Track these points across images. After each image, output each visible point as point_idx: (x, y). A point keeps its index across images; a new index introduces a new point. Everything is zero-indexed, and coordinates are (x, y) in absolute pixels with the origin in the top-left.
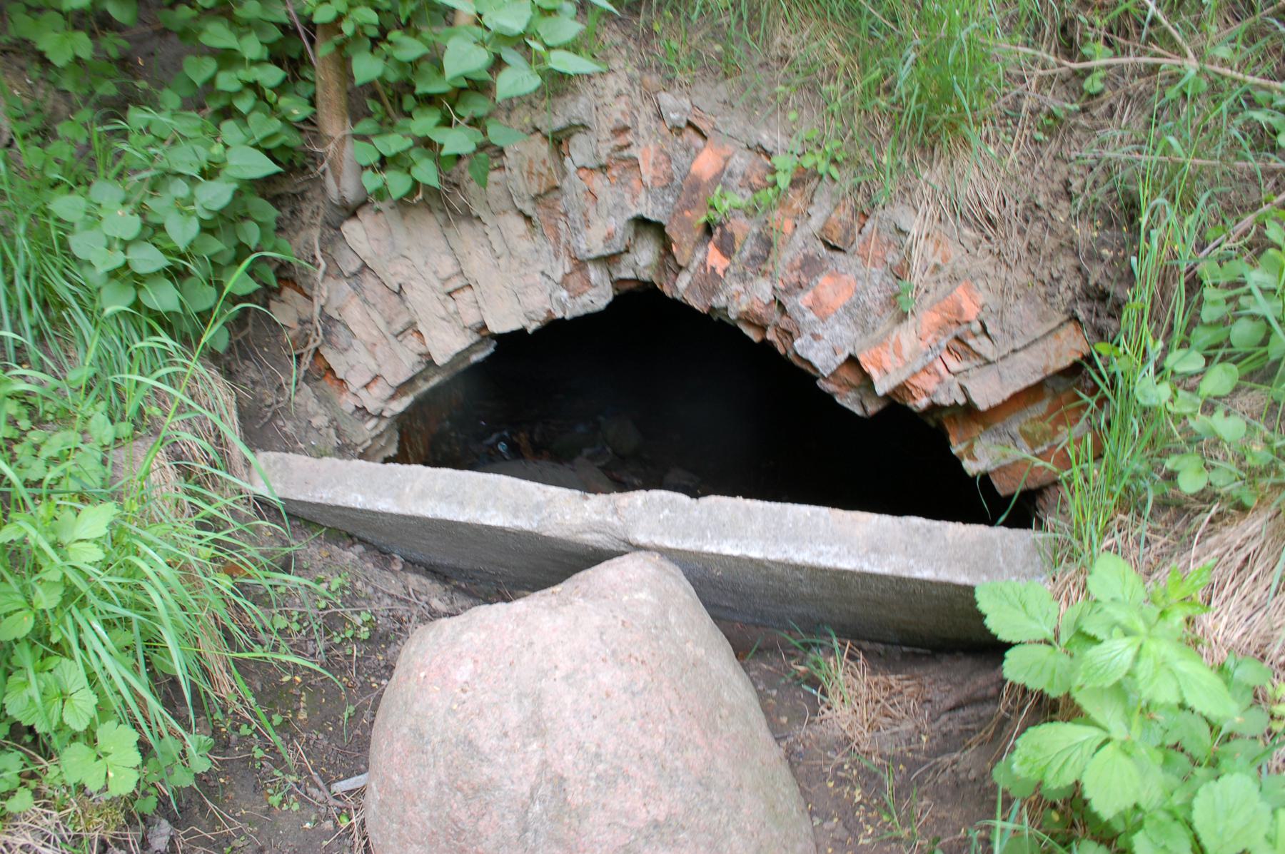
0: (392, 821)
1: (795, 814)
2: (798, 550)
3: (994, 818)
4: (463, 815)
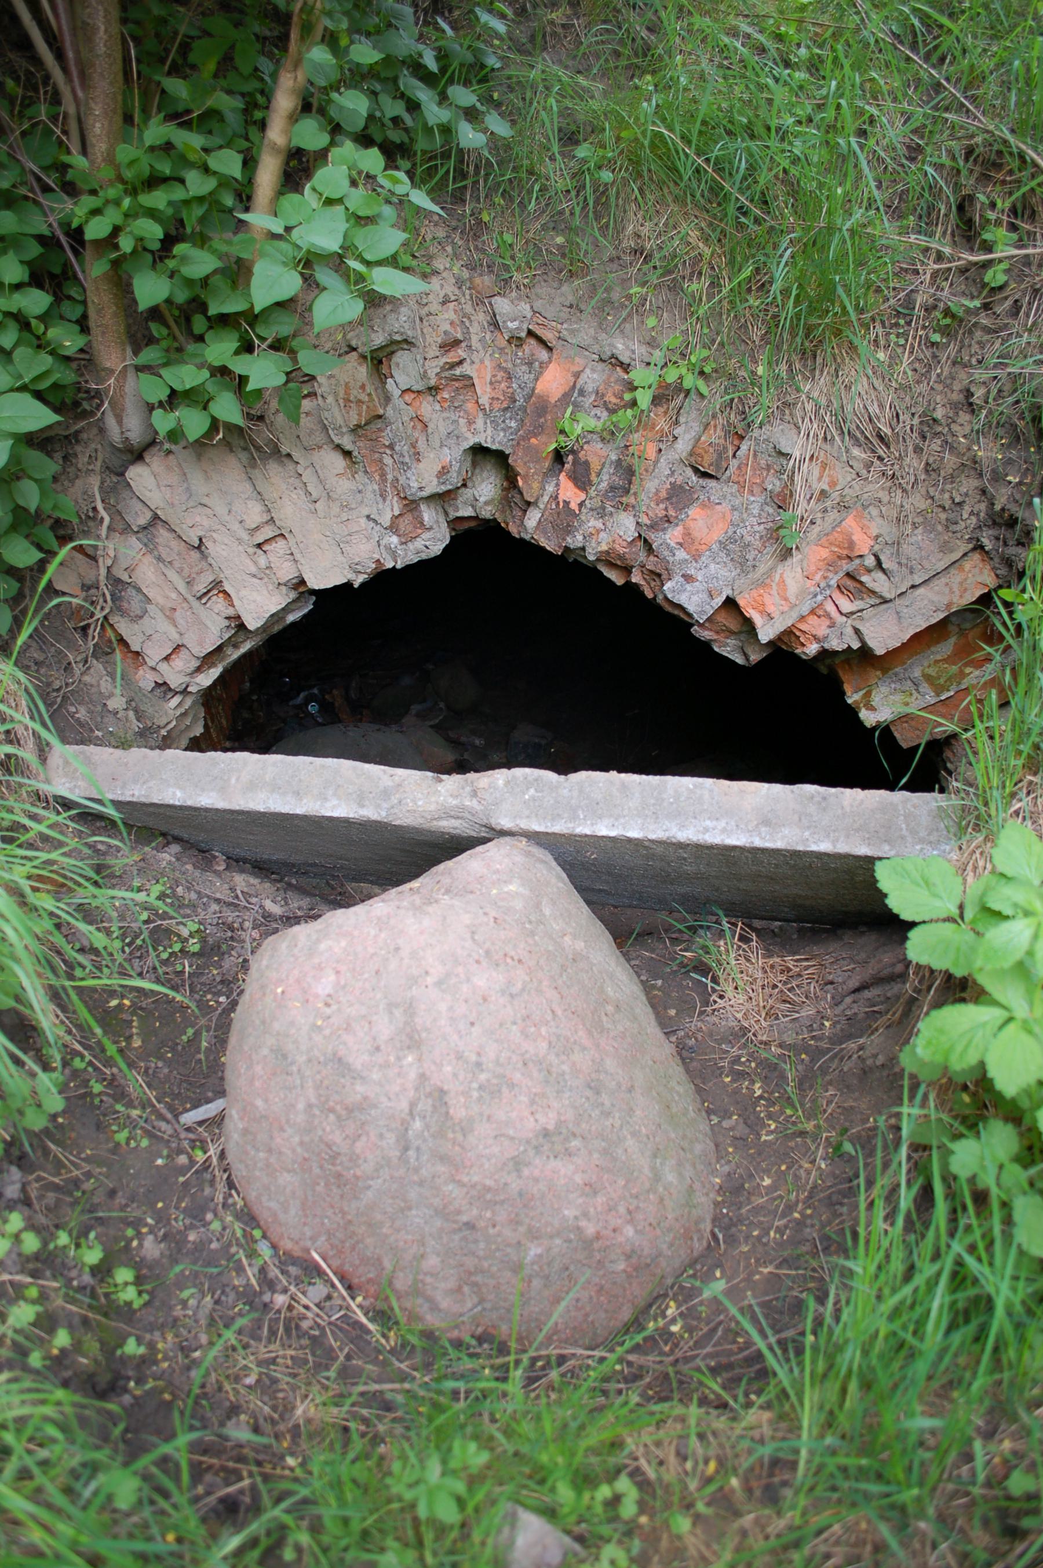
0: (258, 1150)
1: (692, 1114)
2: (682, 827)
3: (901, 1105)
4: (337, 1137)
